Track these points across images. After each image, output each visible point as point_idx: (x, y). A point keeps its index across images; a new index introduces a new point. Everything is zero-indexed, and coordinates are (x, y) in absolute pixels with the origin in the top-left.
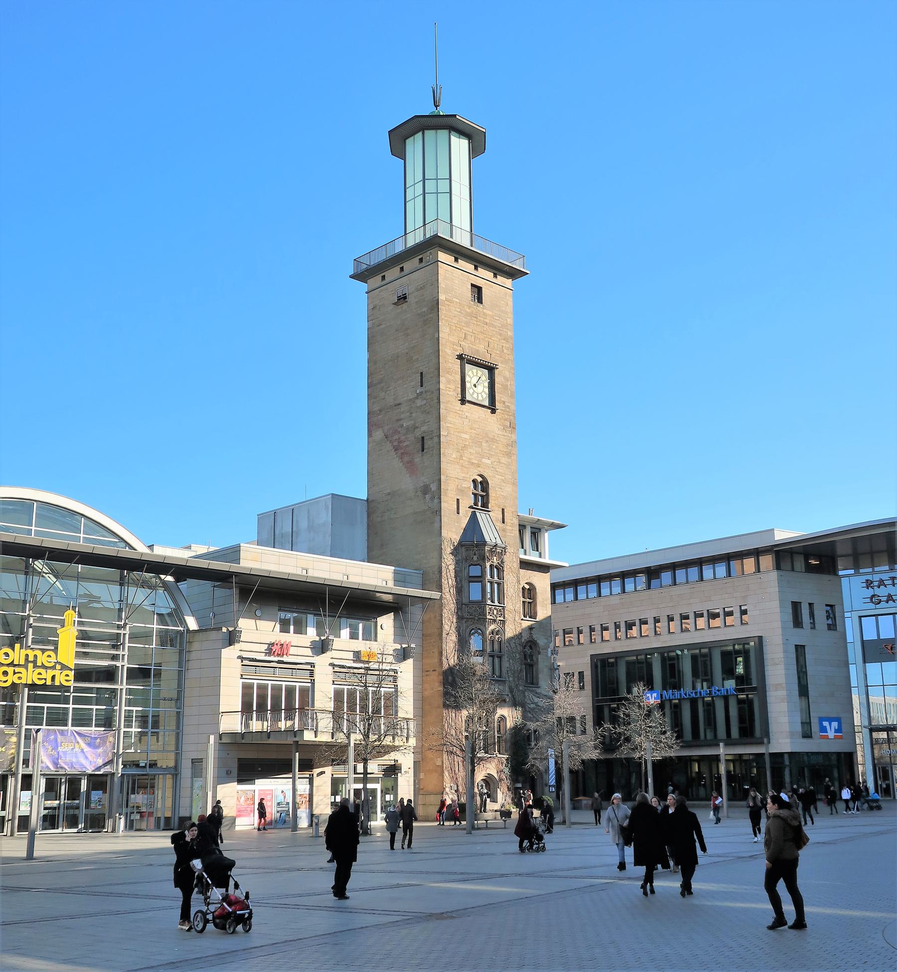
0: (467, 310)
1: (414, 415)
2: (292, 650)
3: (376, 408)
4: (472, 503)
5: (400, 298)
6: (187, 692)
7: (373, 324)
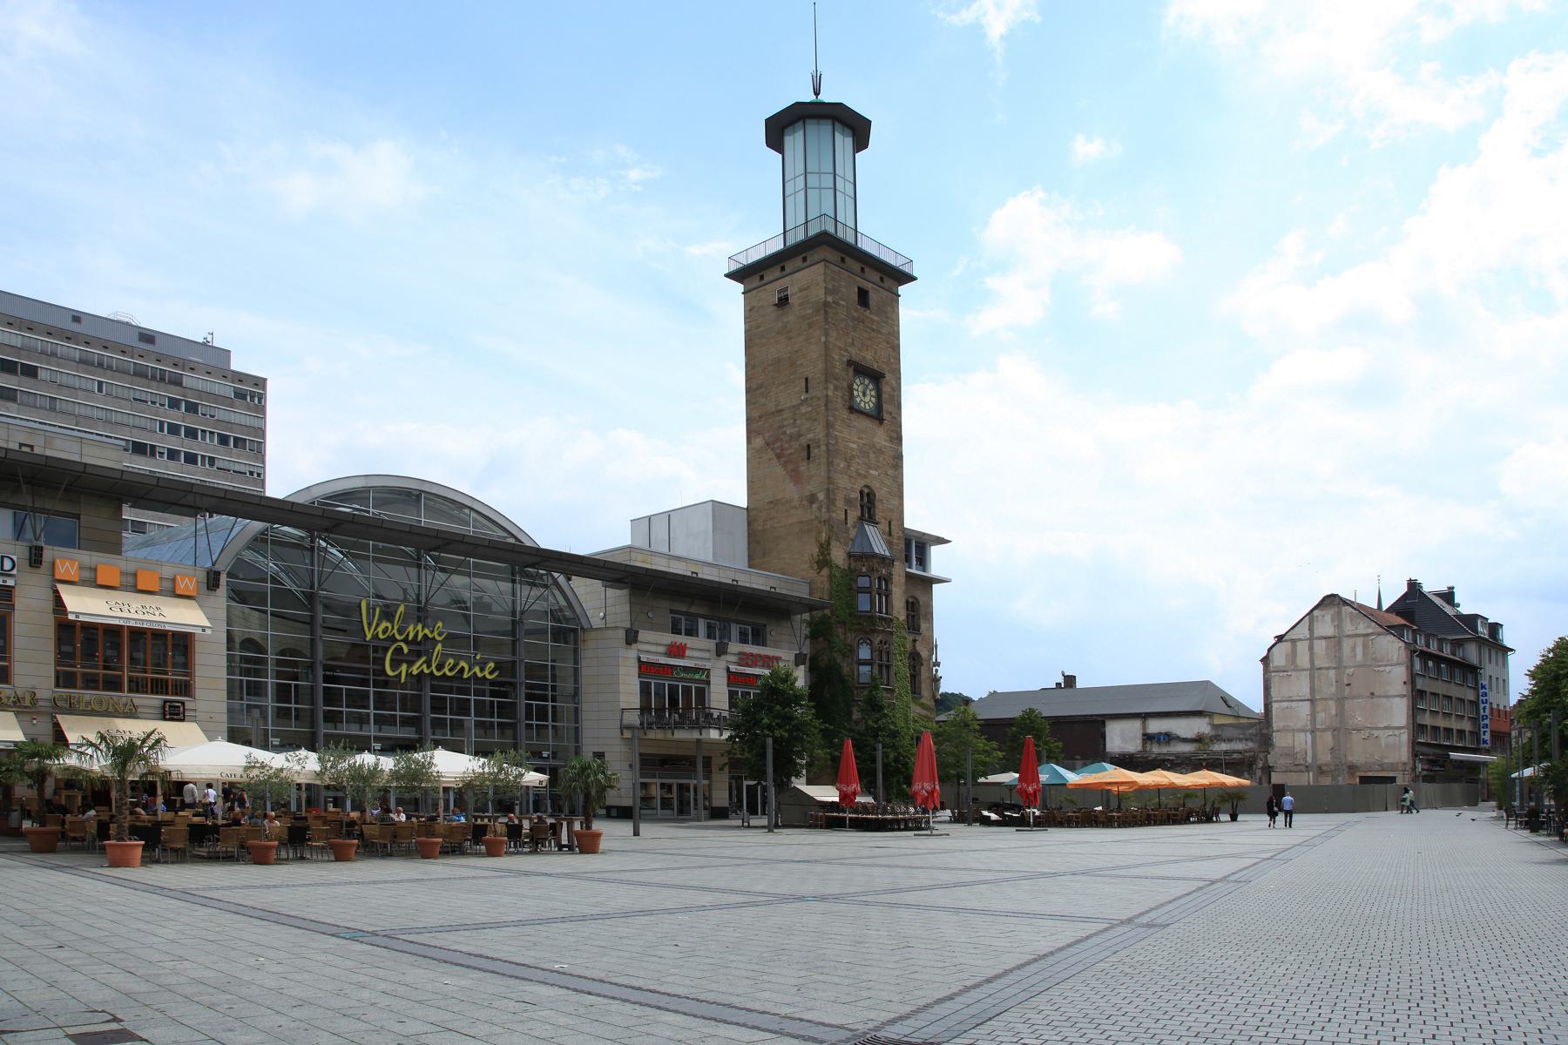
2: (688, 653)
3: (756, 414)
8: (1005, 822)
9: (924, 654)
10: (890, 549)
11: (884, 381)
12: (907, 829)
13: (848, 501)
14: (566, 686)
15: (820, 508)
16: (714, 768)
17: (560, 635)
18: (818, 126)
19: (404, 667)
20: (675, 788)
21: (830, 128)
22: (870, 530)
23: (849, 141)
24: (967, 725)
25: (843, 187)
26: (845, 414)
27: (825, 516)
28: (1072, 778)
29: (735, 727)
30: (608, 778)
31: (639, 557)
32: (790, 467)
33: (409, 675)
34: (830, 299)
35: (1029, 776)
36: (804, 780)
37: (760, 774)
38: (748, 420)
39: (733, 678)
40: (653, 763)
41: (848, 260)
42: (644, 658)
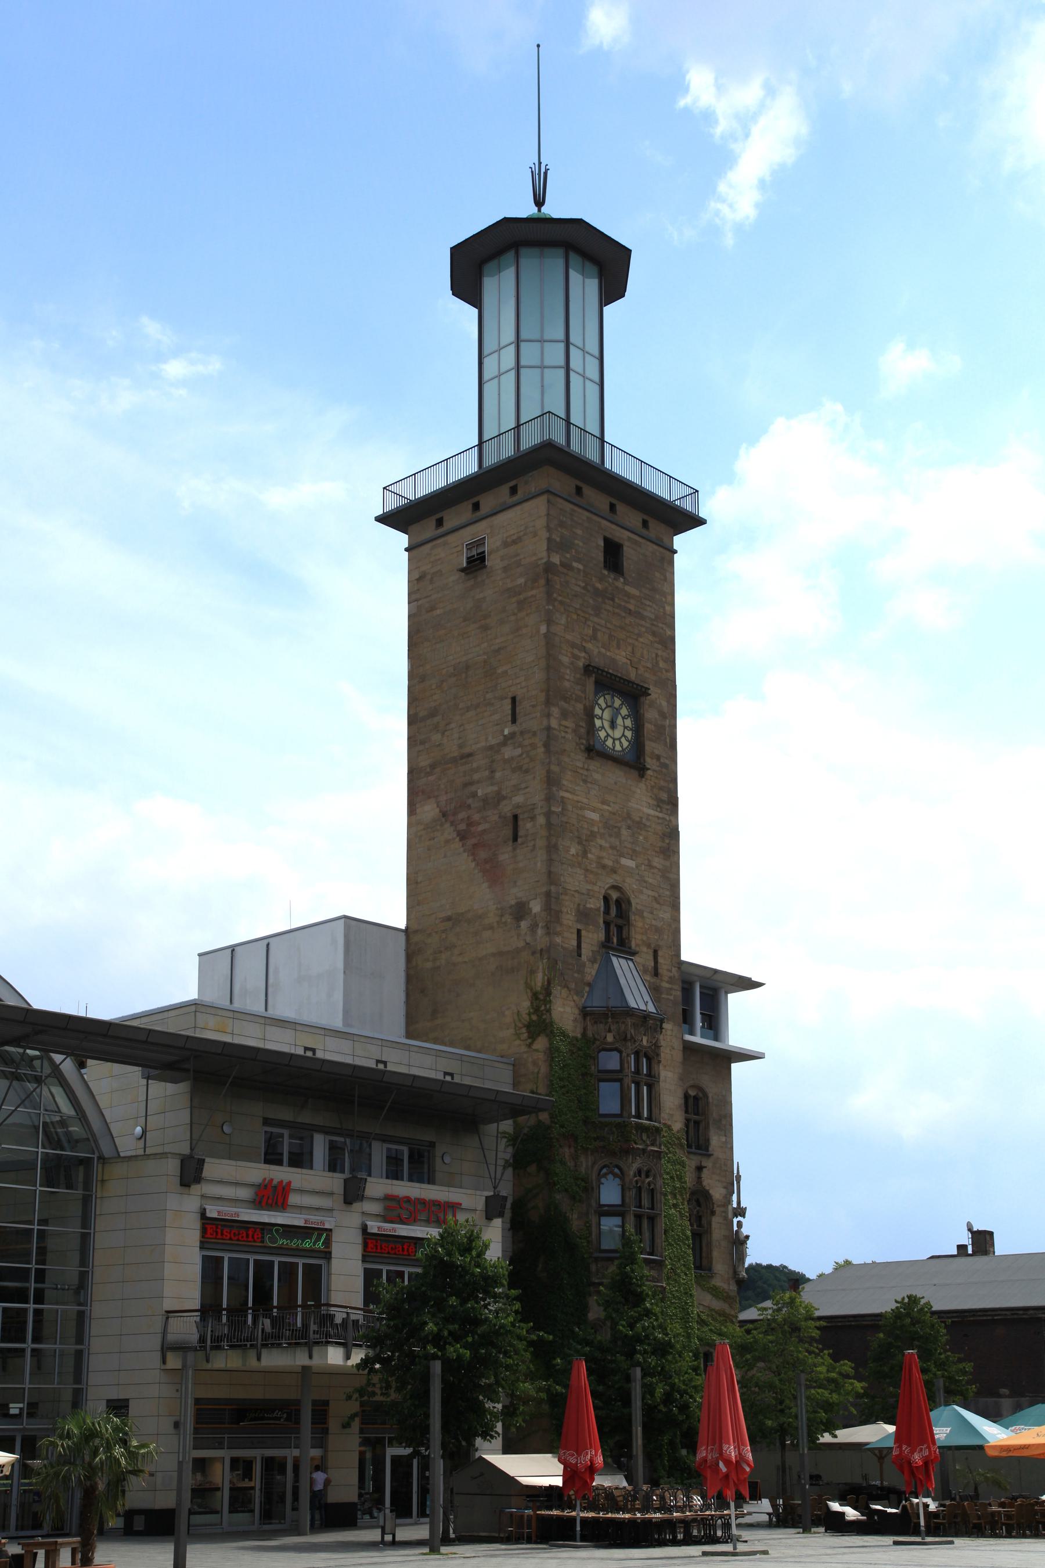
0: (599, 586)
1: (498, 775)
2: (293, 1199)
3: (424, 762)
4: (602, 936)
5: (470, 560)
6: (98, 1274)
7: (419, 607)
8: (873, 1526)
9: (717, 1194)
10: (656, 999)
12: (689, 1541)
13: (584, 915)
14: (64, 1270)
15: (533, 928)
16: (333, 1425)
17: (58, 1172)
18: (543, 262)
20: (257, 1469)
21: (560, 263)
22: (621, 965)
23: (592, 286)
24: (795, 1329)
25: (582, 363)
26: (578, 759)
27: (541, 938)
28: (995, 1434)
29: (374, 1341)
30: (132, 1455)
31: (212, 1022)
32: (483, 854)
34: (556, 559)
35: (914, 1430)
36: (498, 1442)
37: (417, 1434)
38: (410, 772)
39: (373, 1245)
40: (221, 1418)
41: (587, 491)
42: (212, 1213)
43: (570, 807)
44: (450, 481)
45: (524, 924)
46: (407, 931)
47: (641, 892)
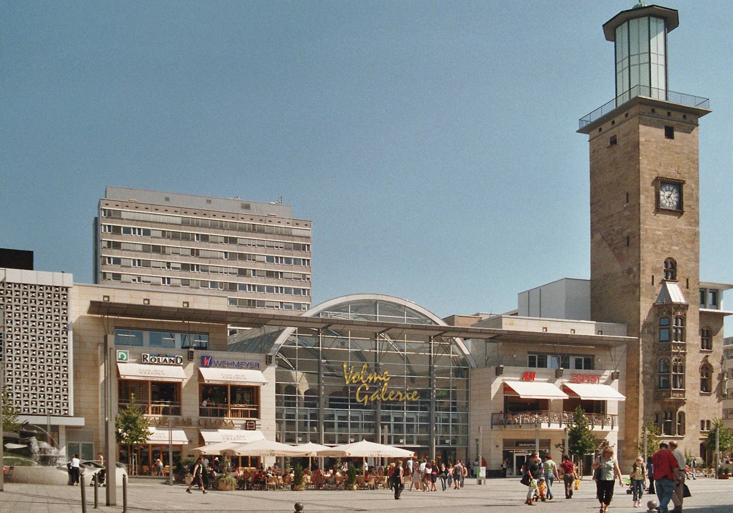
11: (684, 186)
13: (655, 270)
17: (458, 373)
19: (366, 397)
33: (369, 401)
43: (649, 231)
44: (603, 114)
45: (631, 276)
46: (591, 280)
47: (681, 258)
